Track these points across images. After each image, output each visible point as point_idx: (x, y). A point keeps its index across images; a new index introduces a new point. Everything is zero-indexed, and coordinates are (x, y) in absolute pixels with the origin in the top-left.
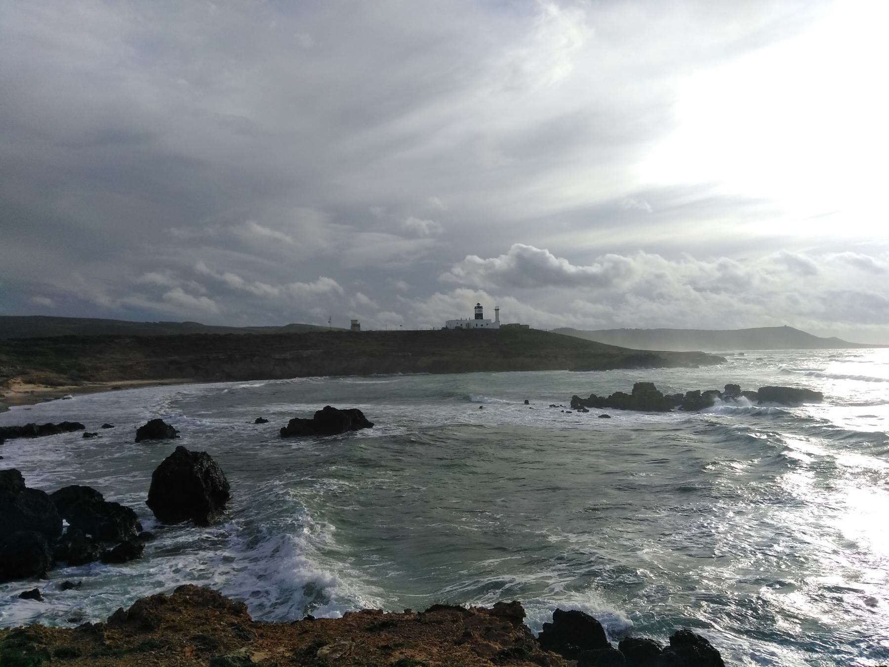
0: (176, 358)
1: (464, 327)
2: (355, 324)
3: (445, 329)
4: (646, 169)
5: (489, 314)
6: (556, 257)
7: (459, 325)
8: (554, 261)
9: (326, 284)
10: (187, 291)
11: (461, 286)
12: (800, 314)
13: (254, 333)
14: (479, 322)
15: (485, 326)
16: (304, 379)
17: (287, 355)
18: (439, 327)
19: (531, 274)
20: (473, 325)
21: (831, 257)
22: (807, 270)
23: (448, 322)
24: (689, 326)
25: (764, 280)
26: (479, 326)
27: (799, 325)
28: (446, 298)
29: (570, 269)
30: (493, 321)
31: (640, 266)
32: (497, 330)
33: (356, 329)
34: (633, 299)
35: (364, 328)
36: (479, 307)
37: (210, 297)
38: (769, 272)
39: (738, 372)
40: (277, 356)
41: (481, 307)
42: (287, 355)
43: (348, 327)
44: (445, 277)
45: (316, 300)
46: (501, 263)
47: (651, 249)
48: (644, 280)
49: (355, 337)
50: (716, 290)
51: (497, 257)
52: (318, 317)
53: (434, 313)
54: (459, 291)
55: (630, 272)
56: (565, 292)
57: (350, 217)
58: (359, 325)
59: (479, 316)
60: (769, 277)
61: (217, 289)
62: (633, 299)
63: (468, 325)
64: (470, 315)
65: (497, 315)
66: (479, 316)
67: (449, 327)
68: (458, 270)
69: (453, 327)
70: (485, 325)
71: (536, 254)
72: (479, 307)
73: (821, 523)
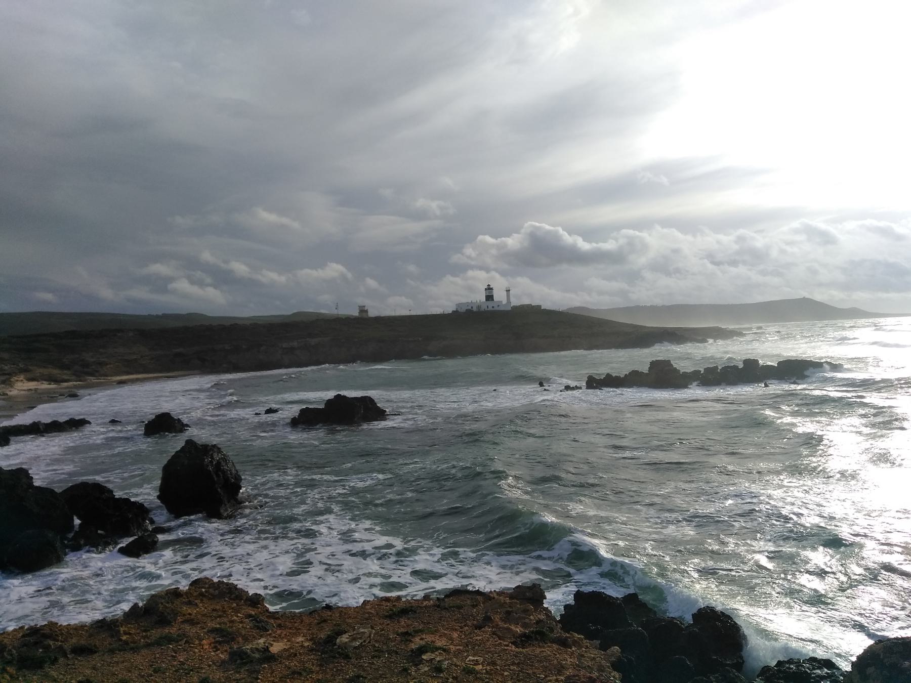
1: (475, 309)
2: (363, 310)
4: (649, 144)
5: (499, 296)
6: (570, 234)
8: (568, 239)
9: (334, 270)
10: (192, 282)
11: (472, 268)
12: (820, 285)
14: (490, 304)
15: (496, 308)
19: (544, 253)
20: (484, 308)
21: (851, 225)
22: (827, 239)
24: (706, 301)
25: (782, 251)
26: (490, 308)
27: (819, 296)
28: (458, 280)
29: (584, 245)
31: (656, 241)
33: (364, 315)
34: (648, 275)
35: (372, 313)
36: (489, 289)
38: (790, 243)
40: (285, 345)
42: (295, 344)
43: (355, 313)
44: (456, 258)
45: (323, 288)
46: (513, 242)
47: (667, 223)
48: (661, 255)
50: (734, 263)
51: (508, 235)
52: (326, 304)
53: (445, 296)
55: (645, 247)
56: (579, 270)
57: (359, 200)
59: (490, 298)
61: (223, 278)
63: (479, 307)
65: (508, 296)
66: (490, 298)
68: (469, 251)
69: (463, 309)
71: (549, 232)
72: (489, 289)
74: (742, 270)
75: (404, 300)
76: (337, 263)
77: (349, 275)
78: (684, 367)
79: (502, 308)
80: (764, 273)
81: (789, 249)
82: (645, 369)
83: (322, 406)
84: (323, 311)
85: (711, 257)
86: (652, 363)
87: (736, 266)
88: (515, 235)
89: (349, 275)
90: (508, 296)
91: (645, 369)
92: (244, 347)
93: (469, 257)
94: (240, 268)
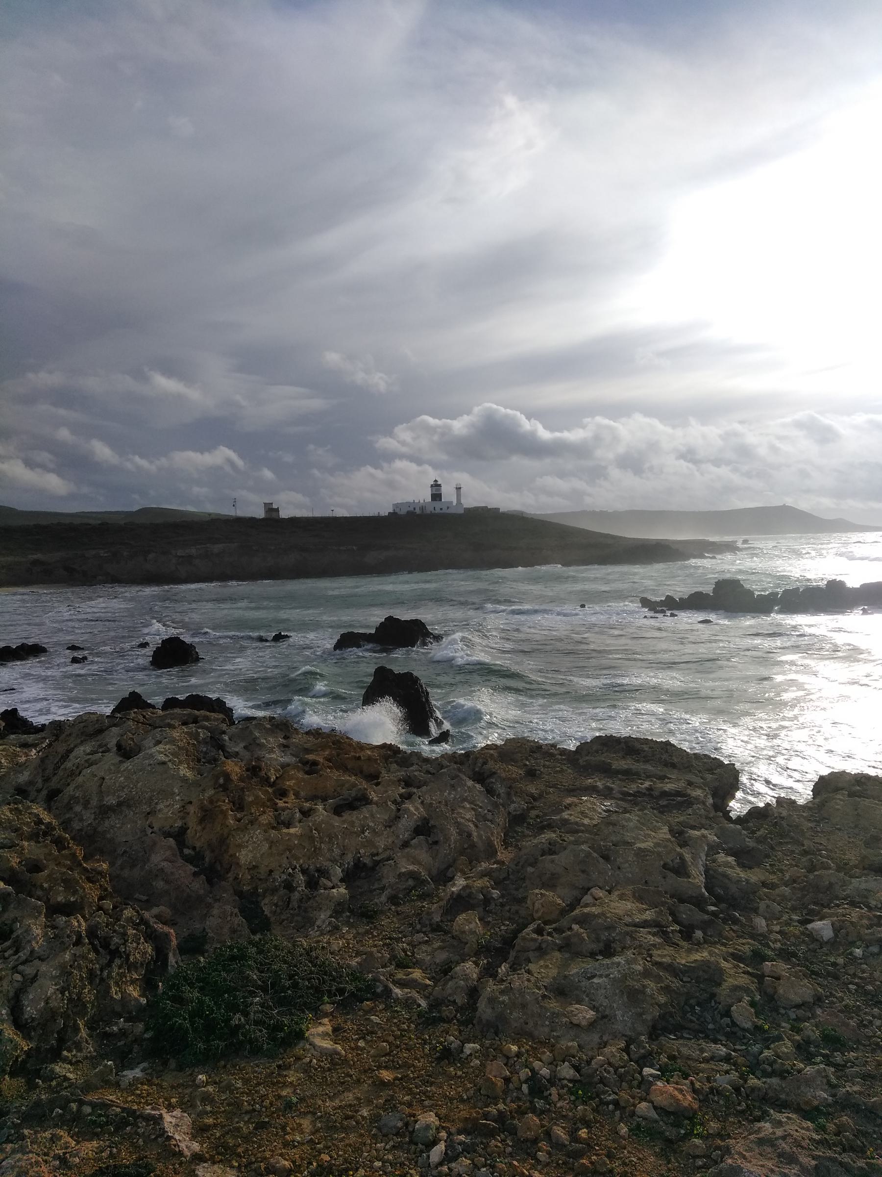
0: (38, 556)
1: (418, 511)
2: (271, 510)
3: (393, 515)
4: (631, 305)
5: (448, 494)
6: (529, 418)
7: (411, 509)
8: (527, 425)
9: (223, 454)
10: (30, 464)
11: (402, 456)
12: (808, 491)
13: (91, 522)
14: (437, 505)
15: (445, 511)
16: (203, 585)
17: (193, 551)
18: (384, 512)
19: (497, 440)
20: (429, 510)
21: (860, 419)
22: (824, 435)
23: (396, 505)
24: (674, 508)
25: (774, 449)
26: (438, 511)
27: (804, 504)
28: (378, 473)
29: (544, 434)
30: (454, 504)
31: (631, 431)
32: (460, 515)
33: (274, 515)
34: (615, 473)
35: (284, 514)
36: (436, 485)
37: (60, 475)
38: (781, 438)
39: (779, 562)
40: (180, 553)
41: (440, 486)
42: (193, 551)
43: (260, 514)
44: (385, 443)
45: (204, 480)
46: (459, 426)
47: (651, 410)
48: (626, 451)
49: (272, 523)
50: (717, 462)
51: (454, 418)
52: (201, 501)
53: (363, 492)
54: (399, 464)
55: (616, 439)
56: (519, 462)
57: (263, 362)
58: (277, 510)
59: (436, 496)
60: (778, 444)
61: (72, 462)
62: (615, 473)
63: (422, 508)
64: (425, 496)
65: (459, 496)
66: (436, 496)
67: (397, 511)
68: (404, 433)
69: (403, 512)
70: (445, 509)
71: (507, 416)
72: (436, 485)
73: (791, 765)
74: (724, 471)
75: (299, 497)
76: (229, 447)
77: (240, 463)
78: (759, 588)
79: (451, 511)
80: (748, 475)
81: (784, 447)
82: (708, 589)
83: (373, 631)
84: (191, 508)
85: (689, 455)
86: (829, 582)
87: (718, 467)
88: (465, 416)
89: (240, 463)
90: (459, 496)
91: (708, 589)
92: (125, 554)
93: (403, 443)
94: (102, 451)
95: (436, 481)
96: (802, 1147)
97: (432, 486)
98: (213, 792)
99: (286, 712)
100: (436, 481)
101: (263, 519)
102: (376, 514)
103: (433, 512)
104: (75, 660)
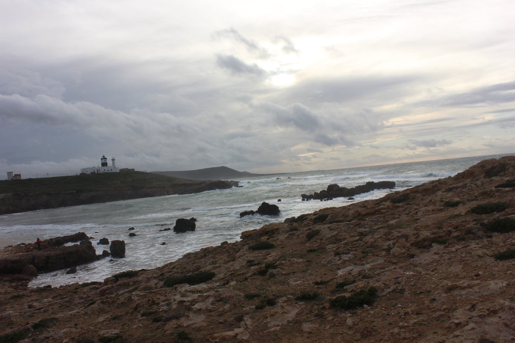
14: (105, 168)
15: (110, 171)
23: (84, 169)
41: (106, 158)
58: (20, 175)
59: (104, 164)
65: (113, 163)
66: (104, 164)
69: (89, 172)
72: (104, 158)
95: (104, 156)
96: (50, 305)
97: (102, 159)
98: (327, 247)
99: (110, 243)
100: (104, 156)
101: (6, 181)
102: (75, 175)
103: (103, 170)
104: (133, 229)
